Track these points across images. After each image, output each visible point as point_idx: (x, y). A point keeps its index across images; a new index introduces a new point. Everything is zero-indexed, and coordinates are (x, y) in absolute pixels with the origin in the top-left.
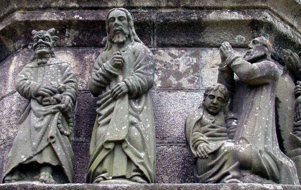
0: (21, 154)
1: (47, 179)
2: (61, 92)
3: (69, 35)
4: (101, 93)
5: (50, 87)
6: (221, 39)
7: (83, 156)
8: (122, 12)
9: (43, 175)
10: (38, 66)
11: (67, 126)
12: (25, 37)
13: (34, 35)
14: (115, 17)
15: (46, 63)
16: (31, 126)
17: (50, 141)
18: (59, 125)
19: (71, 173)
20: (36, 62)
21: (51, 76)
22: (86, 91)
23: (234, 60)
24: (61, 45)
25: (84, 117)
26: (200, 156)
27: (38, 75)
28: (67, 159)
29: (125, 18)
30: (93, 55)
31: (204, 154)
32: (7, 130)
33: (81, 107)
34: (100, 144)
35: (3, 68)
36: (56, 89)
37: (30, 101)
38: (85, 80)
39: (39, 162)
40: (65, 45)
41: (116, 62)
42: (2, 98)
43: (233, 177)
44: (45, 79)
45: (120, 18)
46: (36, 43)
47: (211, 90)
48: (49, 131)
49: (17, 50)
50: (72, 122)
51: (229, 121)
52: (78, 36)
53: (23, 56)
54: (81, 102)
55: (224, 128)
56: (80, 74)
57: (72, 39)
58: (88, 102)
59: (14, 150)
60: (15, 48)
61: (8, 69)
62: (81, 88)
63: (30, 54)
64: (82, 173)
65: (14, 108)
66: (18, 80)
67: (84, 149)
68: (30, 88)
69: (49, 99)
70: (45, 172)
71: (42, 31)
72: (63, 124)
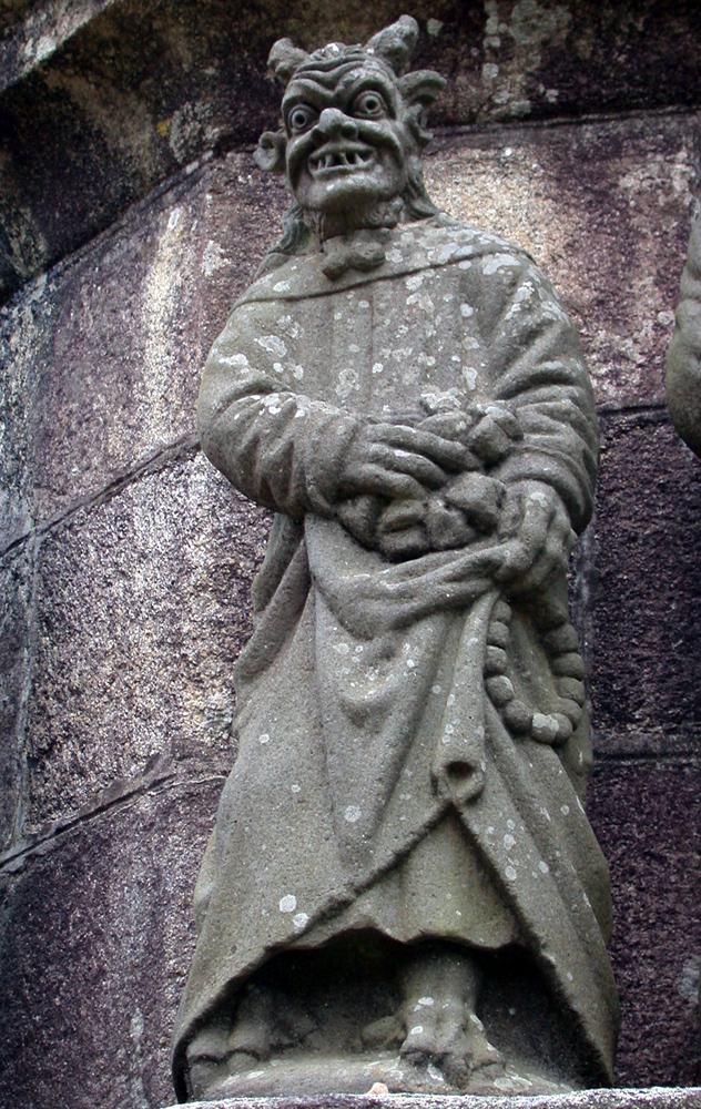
0: (274, 883)
1: (451, 1043)
2: (491, 462)
3: (507, 39)
5: (418, 434)
7: (659, 848)
9: (423, 1019)
10: (329, 286)
11: (549, 673)
12: (226, 78)
13: (287, 74)
15: (378, 262)
16: (319, 700)
17: (447, 796)
18: (494, 681)
19: (598, 984)
20: (310, 258)
21: (416, 352)
22: (647, 414)
24: (464, 115)
25: (642, 584)
27: (338, 352)
28: (568, 903)
30: (672, 162)
32: (169, 701)
33: (625, 524)
35: (101, 282)
36: (459, 446)
37: (298, 532)
38: (635, 341)
39: (388, 931)
40: (488, 113)
42: (113, 484)
44: (380, 375)
46: (302, 131)
48: (439, 726)
49: (180, 167)
50: (575, 650)
52: (569, 41)
53: (227, 207)
54: (617, 489)
56: (601, 303)
57: (530, 63)
58: (662, 487)
59: (227, 860)
60: (168, 154)
61: (137, 289)
62: (612, 391)
63: (266, 189)
64: (661, 962)
65: (199, 554)
66: (215, 392)
67: (663, 798)
68: (291, 445)
69: (422, 512)
70: (436, 992)
71: (334, 47)
72: (520, 668)
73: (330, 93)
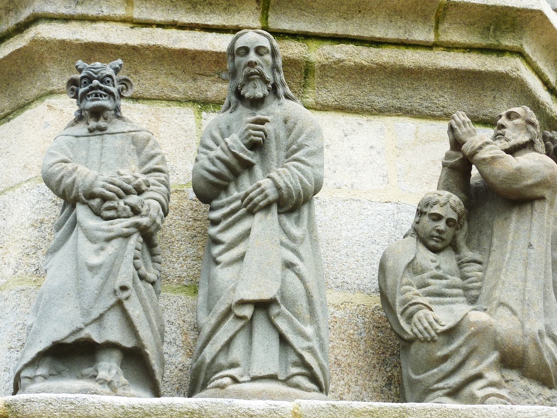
2: (140, 192)
4: (217, 197)
5: (118, 180)
6: (433, 103)
8: (266, 39)
14: (249, 46)
18: (137, 261)
23: (480, 148)
26: (420, 336)
29: (268, 50)
31: (429, 333)
34: (221, 308)
41: (252, 137)
43: (492, 384)
45: (259, 50)
47: (435, 204)
51: (465, 266)
55: (457, 280)
69: (117, 205)
73: (96, 76)
